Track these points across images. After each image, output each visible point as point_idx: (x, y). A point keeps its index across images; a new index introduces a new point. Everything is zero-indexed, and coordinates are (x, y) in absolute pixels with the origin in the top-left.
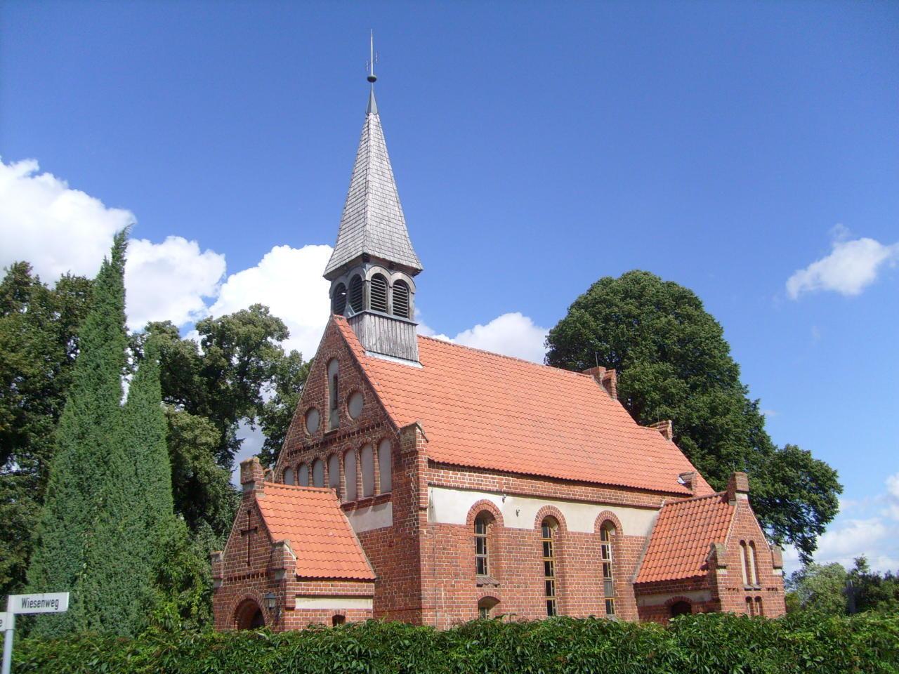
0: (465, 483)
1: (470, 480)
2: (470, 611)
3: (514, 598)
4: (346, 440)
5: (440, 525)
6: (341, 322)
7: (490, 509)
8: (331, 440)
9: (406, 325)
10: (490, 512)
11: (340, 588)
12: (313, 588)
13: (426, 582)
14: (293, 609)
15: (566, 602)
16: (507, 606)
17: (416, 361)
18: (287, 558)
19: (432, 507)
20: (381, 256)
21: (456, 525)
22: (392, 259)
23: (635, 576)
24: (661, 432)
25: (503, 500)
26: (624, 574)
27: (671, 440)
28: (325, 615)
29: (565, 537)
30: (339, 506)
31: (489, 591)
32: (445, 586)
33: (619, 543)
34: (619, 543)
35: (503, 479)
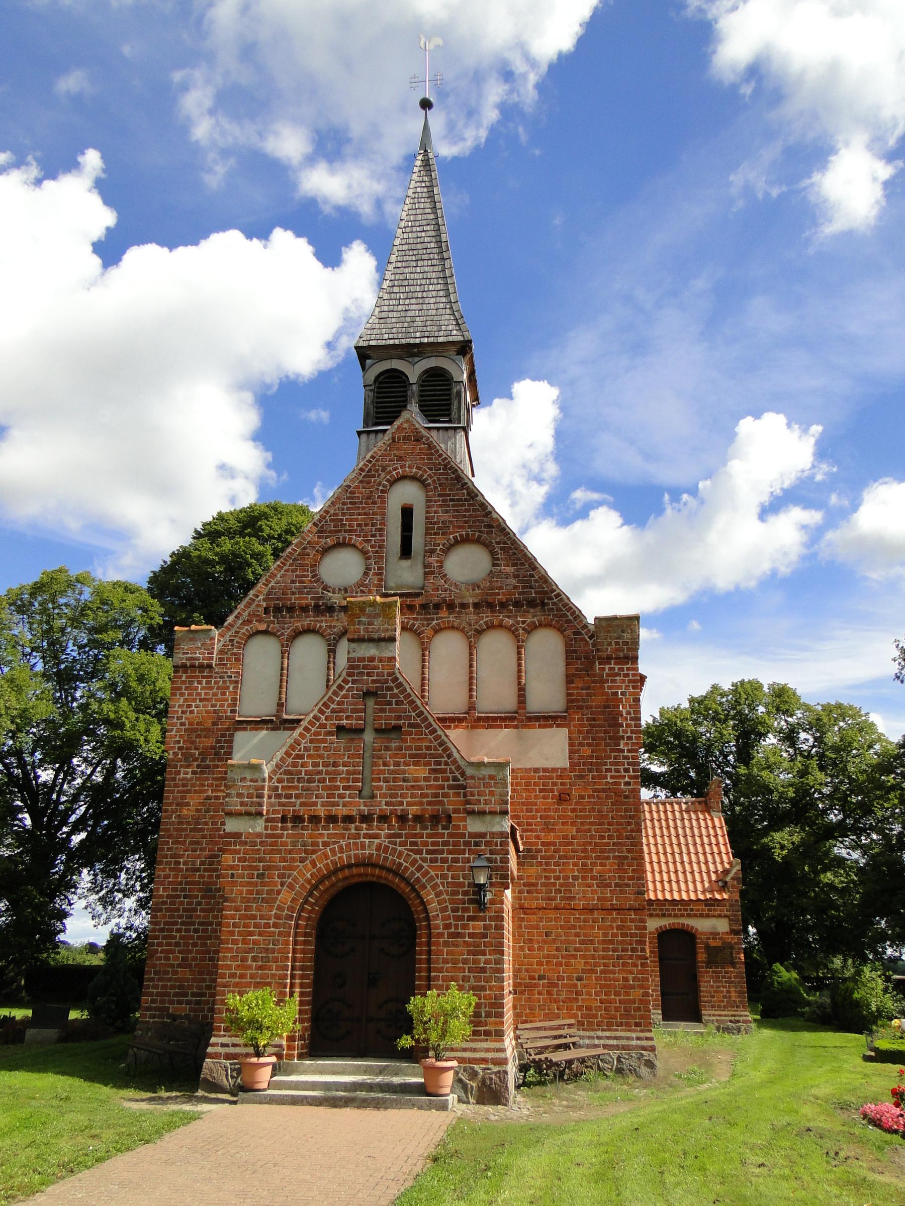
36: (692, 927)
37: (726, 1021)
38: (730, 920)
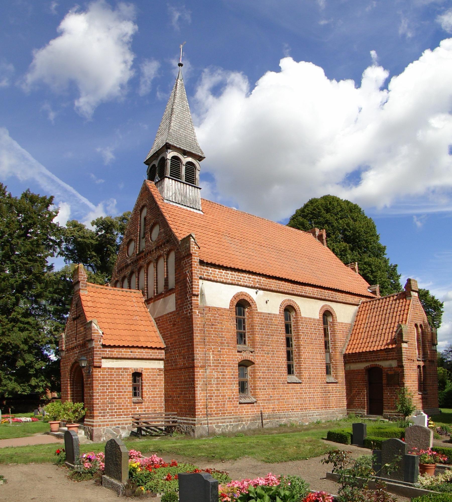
0: (228, 279)
1: (232, 277)
2: (232, 369)
3: (264, 362)
4: (148, 256)
5: (209, 308)
6: (151, 184)
7: (246, 299)
8: (140, 258)
9: (193, 188)
10: (247, 301)
11: (137, 353)
12: (115, 352)
13: (198, 348)
14: (100, 367)
15: (300, 366)
16: (259, 367)
17: (199, 210)
18: (94, 333)
19: (202, 295)
20: (178, 146)
21: (222, 309)
22: (185, 149)
23: (344, 349)
24: (352, 269)
25: (256, 293)
26: (338, 348)
27: (357, 273)
28: (126, 372)
29: (300, 321)
30: (144, 301)
31: (246, 356)
32: (213, 351)
33: (334, 327)
34: (334, 327)
35: (256, 279)
36: (381, 366)
37: (394, 415)
38: (398, 361)
